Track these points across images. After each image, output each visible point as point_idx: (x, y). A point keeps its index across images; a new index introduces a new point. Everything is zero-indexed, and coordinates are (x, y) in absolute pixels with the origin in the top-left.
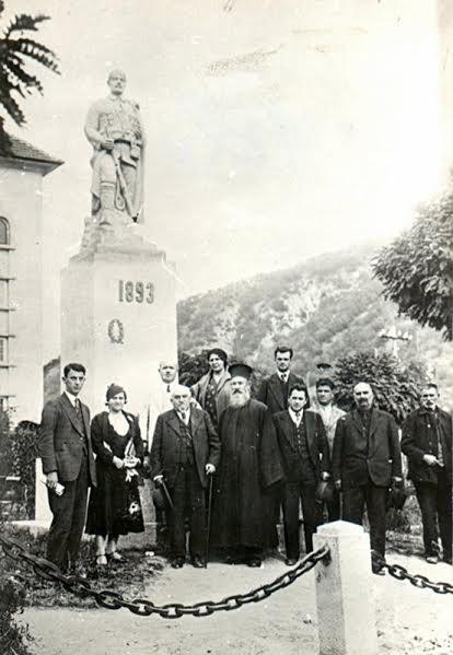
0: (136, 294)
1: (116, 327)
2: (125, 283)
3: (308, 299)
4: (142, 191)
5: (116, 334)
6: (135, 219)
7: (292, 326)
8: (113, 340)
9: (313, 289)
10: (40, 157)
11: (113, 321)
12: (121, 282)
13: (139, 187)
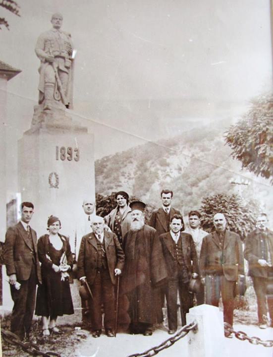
0: (67, 155)
1: (54, 178)
6: (67, 106)
7: (173, 176)
10: (6, 68)
12: (57, 147)
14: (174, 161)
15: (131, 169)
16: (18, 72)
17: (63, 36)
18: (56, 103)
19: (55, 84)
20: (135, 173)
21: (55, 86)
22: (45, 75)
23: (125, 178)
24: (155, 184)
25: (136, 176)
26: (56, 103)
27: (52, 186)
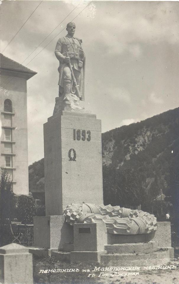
0: (82, 137)
1: (72, 153)
2: (76, 130)
3: (146, 138)
4: (84, 83)
5: (72, 156)
6: (81, 99)
7: (139, 150)
8: (71, 159)
9: (148, 133)
10: (25, 70)
11: (71, 150)
12: (74, 130)
13: (82, 82)
14: (140, 140)
15: (111, 145)
16: (34, 73)
17: (76, 42)
18: (72, 95)
19: (71, 81)
20: (114, 148)
21: (71, 82)
22: (64, 73)
23: (107, 151)
24: (127, 155)
25: (115, 150)
26: (72, 95)
27: (71, 159)
